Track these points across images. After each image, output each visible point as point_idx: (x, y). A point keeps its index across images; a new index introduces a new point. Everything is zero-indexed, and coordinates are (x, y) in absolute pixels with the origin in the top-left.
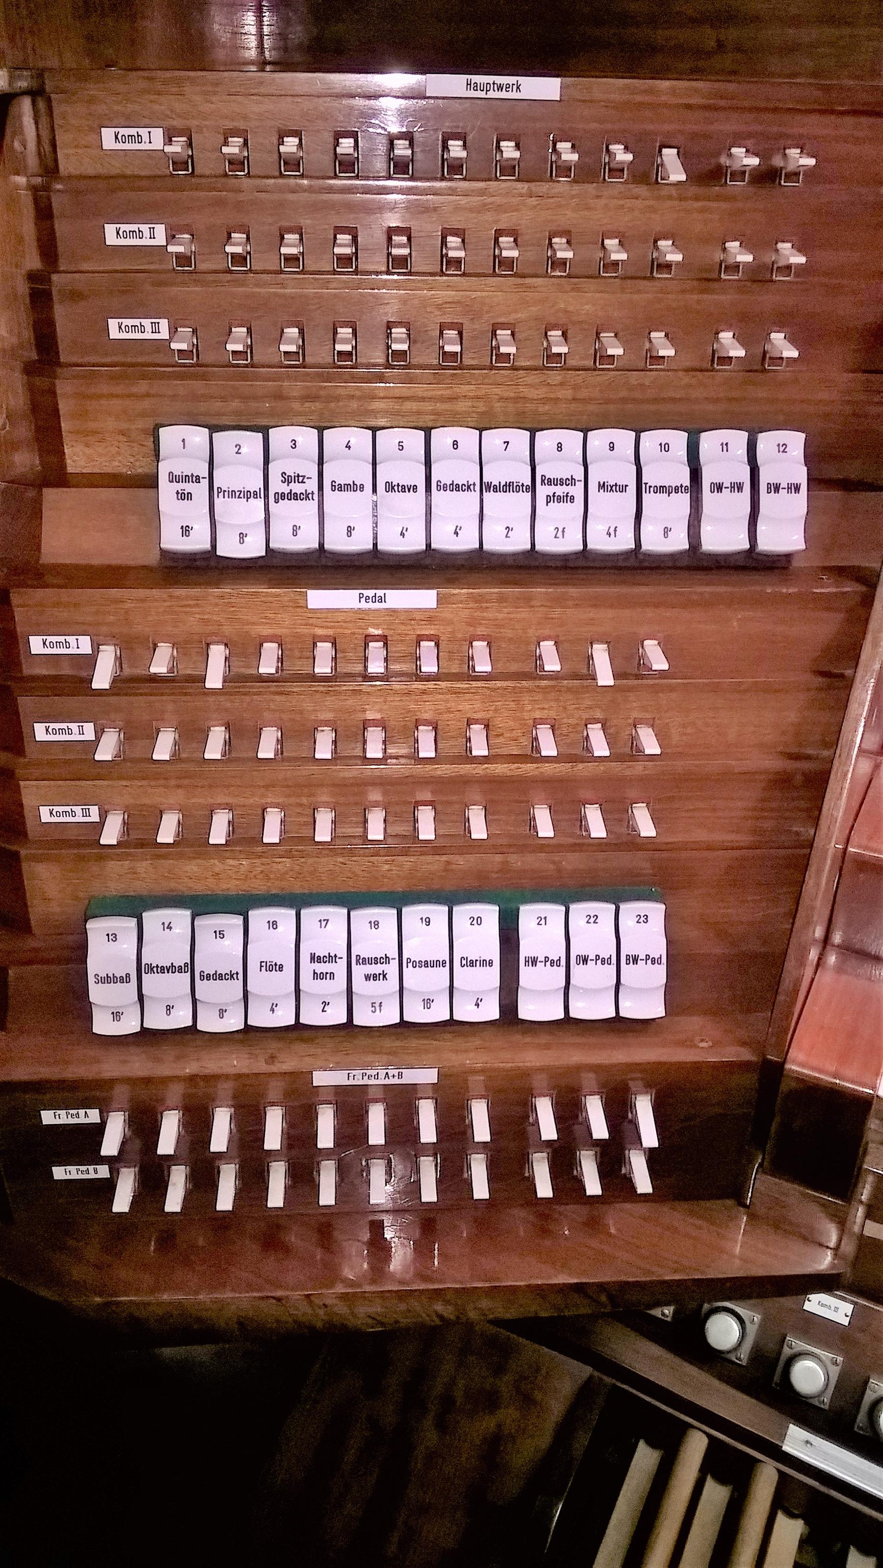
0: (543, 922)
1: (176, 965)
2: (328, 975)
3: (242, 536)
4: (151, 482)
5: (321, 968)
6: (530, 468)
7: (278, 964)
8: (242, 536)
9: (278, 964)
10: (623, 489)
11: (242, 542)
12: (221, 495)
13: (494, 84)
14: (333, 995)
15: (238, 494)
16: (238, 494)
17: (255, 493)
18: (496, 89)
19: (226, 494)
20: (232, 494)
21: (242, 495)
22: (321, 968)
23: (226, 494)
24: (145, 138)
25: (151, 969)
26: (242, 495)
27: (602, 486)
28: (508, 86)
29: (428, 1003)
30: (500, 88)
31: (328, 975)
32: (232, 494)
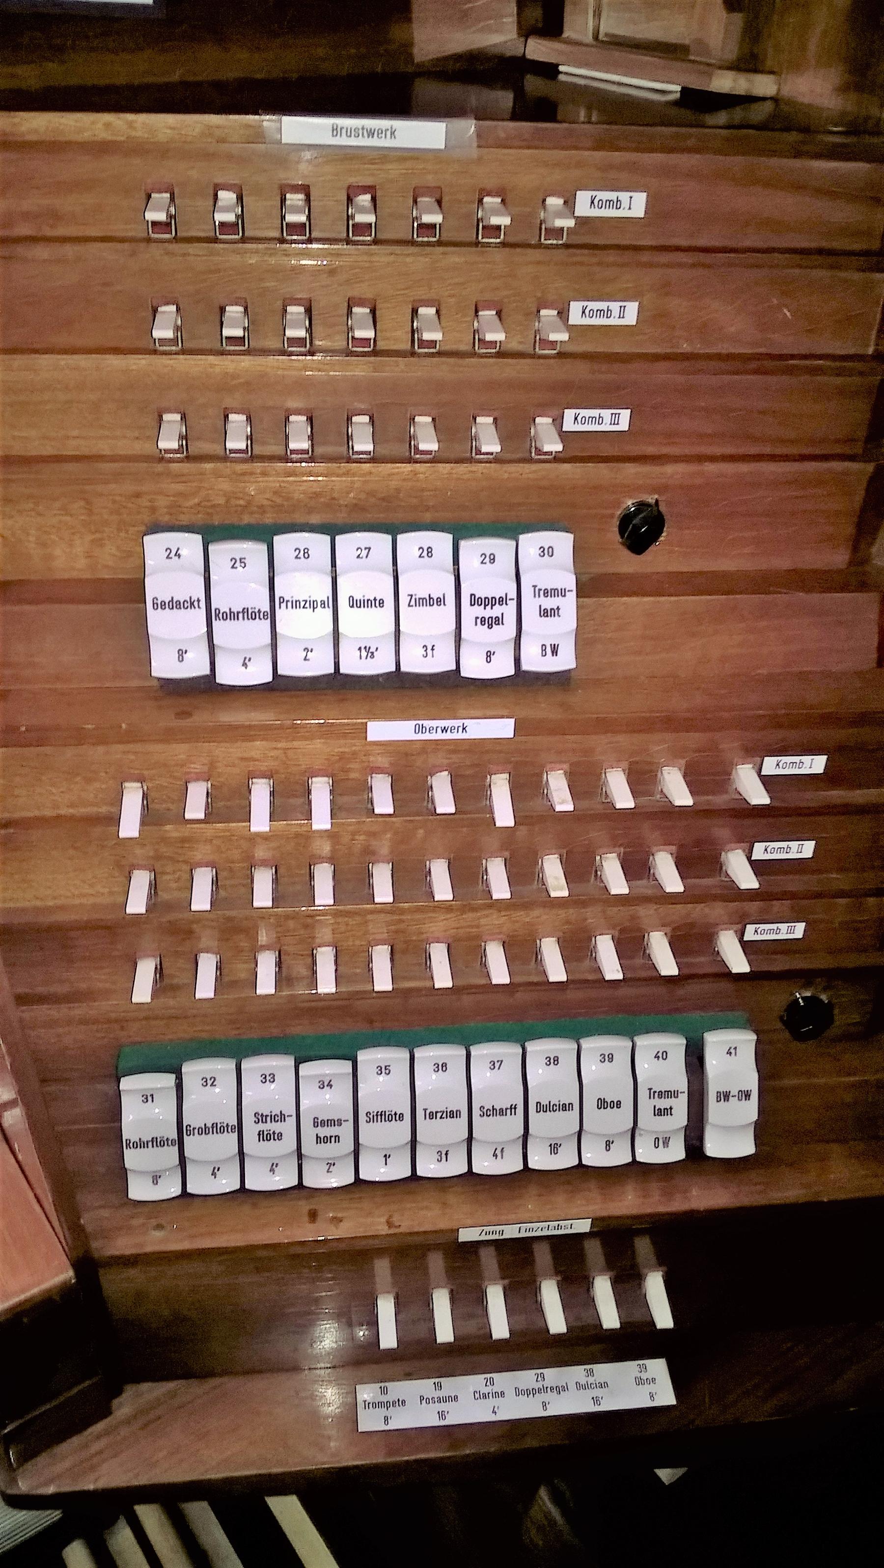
0: (150, 1099)
1: (497, 1107)
2: (333, 1139)
3: (181, 654)
4: (582, 591)
5: (324, 1132)
6: (453, 578)
7: (277, 1132)
8: (181, 654)
9: (277, 1132)
10: (440, 601)
11: (181, 658)
12: (283, 605)
13: (363, 129)
14: (564, 1138)
15: (302, 604)
16: (302, 604)
17: (323, 603)
18: (365, 134)
19: (290, 604)
20: (296, 604)
21: (307, 605)
22: (324, 1132)
23: (290, 604)
24: (625, 203)
25: (173, 1143)
26: (307, 605)
27: (354, 603)
28: (380, 132)
29: (554, 1148)
30: (371, 133)
31: (333, 1139)
32: (296, 604)
